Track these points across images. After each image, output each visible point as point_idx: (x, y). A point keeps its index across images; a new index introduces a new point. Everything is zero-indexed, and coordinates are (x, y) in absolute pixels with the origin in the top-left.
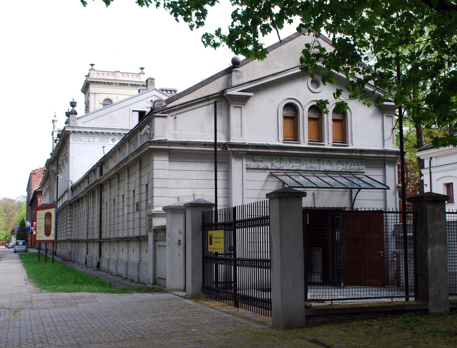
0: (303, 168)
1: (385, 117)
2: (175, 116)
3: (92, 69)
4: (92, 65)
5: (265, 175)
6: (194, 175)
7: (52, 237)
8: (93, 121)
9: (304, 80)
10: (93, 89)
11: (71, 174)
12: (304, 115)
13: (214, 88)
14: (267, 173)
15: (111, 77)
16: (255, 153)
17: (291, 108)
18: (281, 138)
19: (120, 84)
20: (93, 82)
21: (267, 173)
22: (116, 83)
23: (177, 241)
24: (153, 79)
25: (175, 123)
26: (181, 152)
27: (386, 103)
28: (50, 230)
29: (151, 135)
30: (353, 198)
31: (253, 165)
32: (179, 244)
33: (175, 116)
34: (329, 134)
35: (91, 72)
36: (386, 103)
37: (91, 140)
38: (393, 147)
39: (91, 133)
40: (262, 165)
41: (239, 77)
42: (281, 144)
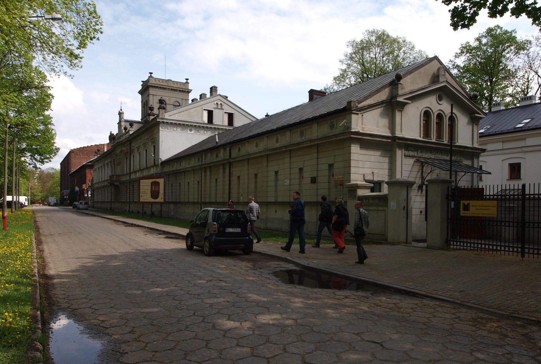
3: (151, 76)
4: (151, 73)
6: (373, 158)
7: (160, 199)
8: (176, 115)
9: (434, 95)
10: (152, 91)
11: (160, 154)
12: (434, 119)
14: (414, 160)
15: (165, 84)
16: (408, 145)
17: (427, 114)
18: (422, 136)
19: (172, 89)
20: (152, 86)
21: (414, 160)
22: (169, 89)
23: (402, 207)
24: (216, 88)
25: (362, 119)
26: (369, 142)
27: (476, 115)
28: (158, 194)
29: (349, 127)
31: (407, 153)
32: (404, 209)
35: (150, 78)
36: (476, 115)
37: (175, 129)
39: (176, 124)
40: (411, 153)
41: (402, 89)
42: (421, 139)
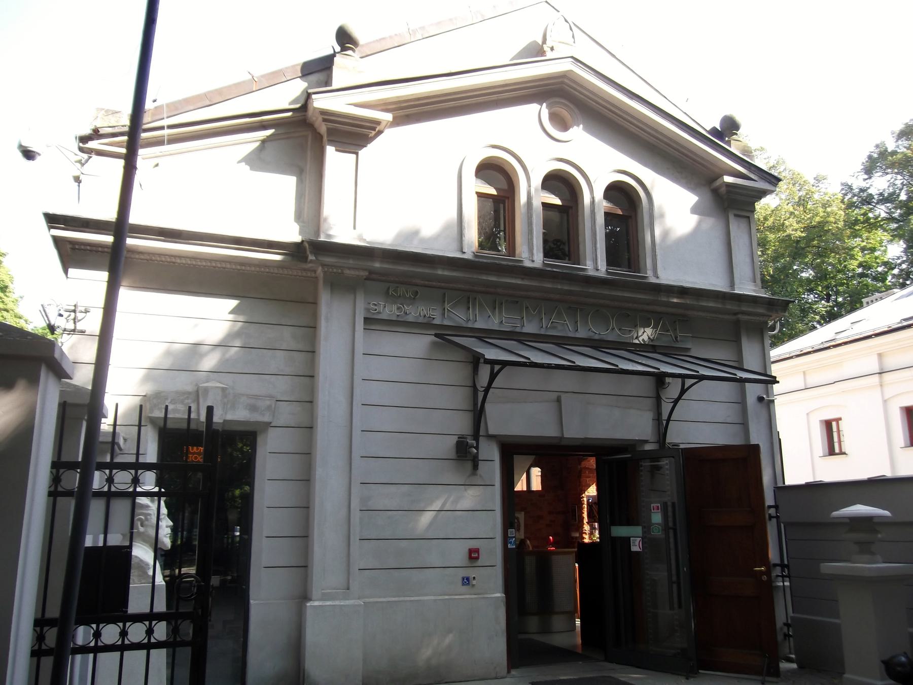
0: (530, 328)
1: (731, 217)
2: (155, 161)
5: (419, 344)
13: (283, 97)
30: (665, 416)
31: (389, 311)
33: (155, 161)
34: (598, 245)
38: (754, 291)
40: (415, 312)
